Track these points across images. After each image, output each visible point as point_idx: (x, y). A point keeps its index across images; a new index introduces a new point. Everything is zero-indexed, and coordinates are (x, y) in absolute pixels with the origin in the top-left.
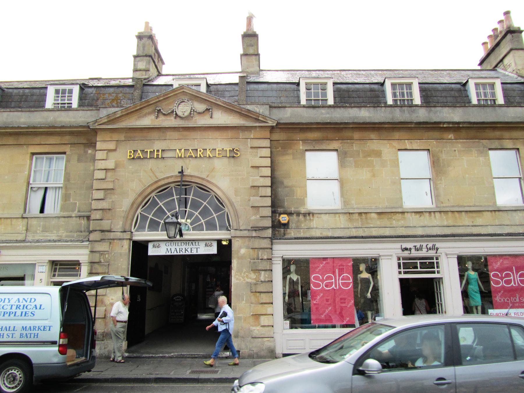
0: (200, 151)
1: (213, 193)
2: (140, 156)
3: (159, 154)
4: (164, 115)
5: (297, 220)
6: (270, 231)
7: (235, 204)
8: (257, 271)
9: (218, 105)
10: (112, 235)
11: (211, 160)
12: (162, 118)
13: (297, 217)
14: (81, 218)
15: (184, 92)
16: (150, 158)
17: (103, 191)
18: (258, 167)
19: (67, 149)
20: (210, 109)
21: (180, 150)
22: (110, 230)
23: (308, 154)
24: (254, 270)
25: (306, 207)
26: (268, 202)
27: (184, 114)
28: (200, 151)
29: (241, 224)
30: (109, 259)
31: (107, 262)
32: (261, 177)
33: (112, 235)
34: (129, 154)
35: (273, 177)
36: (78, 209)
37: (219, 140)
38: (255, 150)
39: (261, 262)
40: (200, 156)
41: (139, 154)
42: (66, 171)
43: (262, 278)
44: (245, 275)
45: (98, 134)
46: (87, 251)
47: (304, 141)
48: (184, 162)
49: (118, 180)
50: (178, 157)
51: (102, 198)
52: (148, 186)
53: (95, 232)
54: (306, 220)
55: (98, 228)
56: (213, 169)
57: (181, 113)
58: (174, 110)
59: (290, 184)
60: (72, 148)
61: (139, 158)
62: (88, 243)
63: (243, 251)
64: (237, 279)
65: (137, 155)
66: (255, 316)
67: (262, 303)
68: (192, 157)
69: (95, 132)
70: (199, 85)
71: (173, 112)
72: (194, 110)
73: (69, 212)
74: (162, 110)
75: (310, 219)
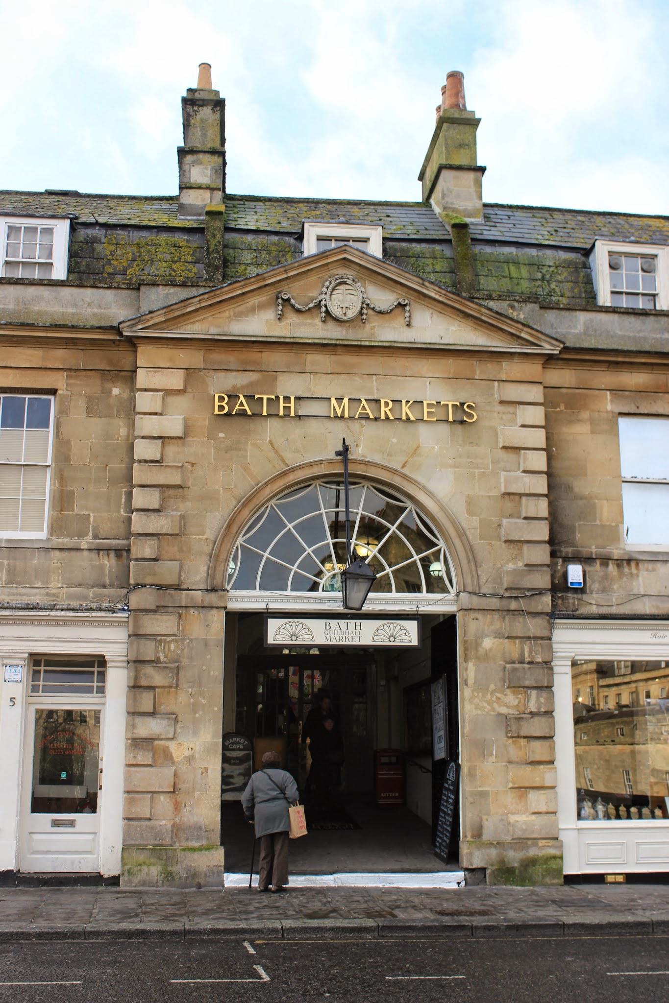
0: (387, 404)
1: (410, 505)
2: (245, 410)
3: (289, 407)
4: (298, 311)
5: (602, 574)
6: (547, 599)
7: (468, 532)
8: (516, 686)
9: (426, 296)
10: (183, 598)
11: (411, 428)
12: (292, 318)
13: (603, 568)
14: (101, 553)
15: (344, 259)
16: (269, 415)
17: (157, 490)
18: (517, 449)
19: (58, 381)
20: (405, 305)
21: (340, 400)
22: (178, 585)
23: (624, 424)
24: (514, 687)
25: (621, 546)
26: (542, 532)
27: (345, 314)
28: (387, 404)
29: (483, 580)
30: (178, 654)
31: (174, 662)
32: (525, 472)
33: (183, 598)
34: (217, 403)
35: (554, 519)
36: (93, 530)
37: (428, 380)
38: (510, 409)
39: (529, 668)
40: (387, 418)
41: (242, 404)
42: (60, 437)
43: (533, 706)
44: (494, 699)
45: (139, 349)
46: (120, 634)
47: (617, 391)
48: (348, 427)
49: (192, 464)
50: (336, 417)
51: (156, 506)
52: (266, 483)
53: (144, 589)
54: (621, 575)
55: (148, 580)
56: (416, 450)
57: (340, 310)
58: (323, 303)
59: (586, 492)
60: (72, 381)
61: (242, 414)
62: (126, 614)
63: (488, 643)
64: (477, 707)
65: (237, 407)
66: (517, 790)
67: (533, 763)
68: (367, 417)
69: (132, 343)
70: (366, 240)
71: (318, 306)
72: (368, 305)
73: (73, 537)
74: (293, 301)
75: (631, 574)
